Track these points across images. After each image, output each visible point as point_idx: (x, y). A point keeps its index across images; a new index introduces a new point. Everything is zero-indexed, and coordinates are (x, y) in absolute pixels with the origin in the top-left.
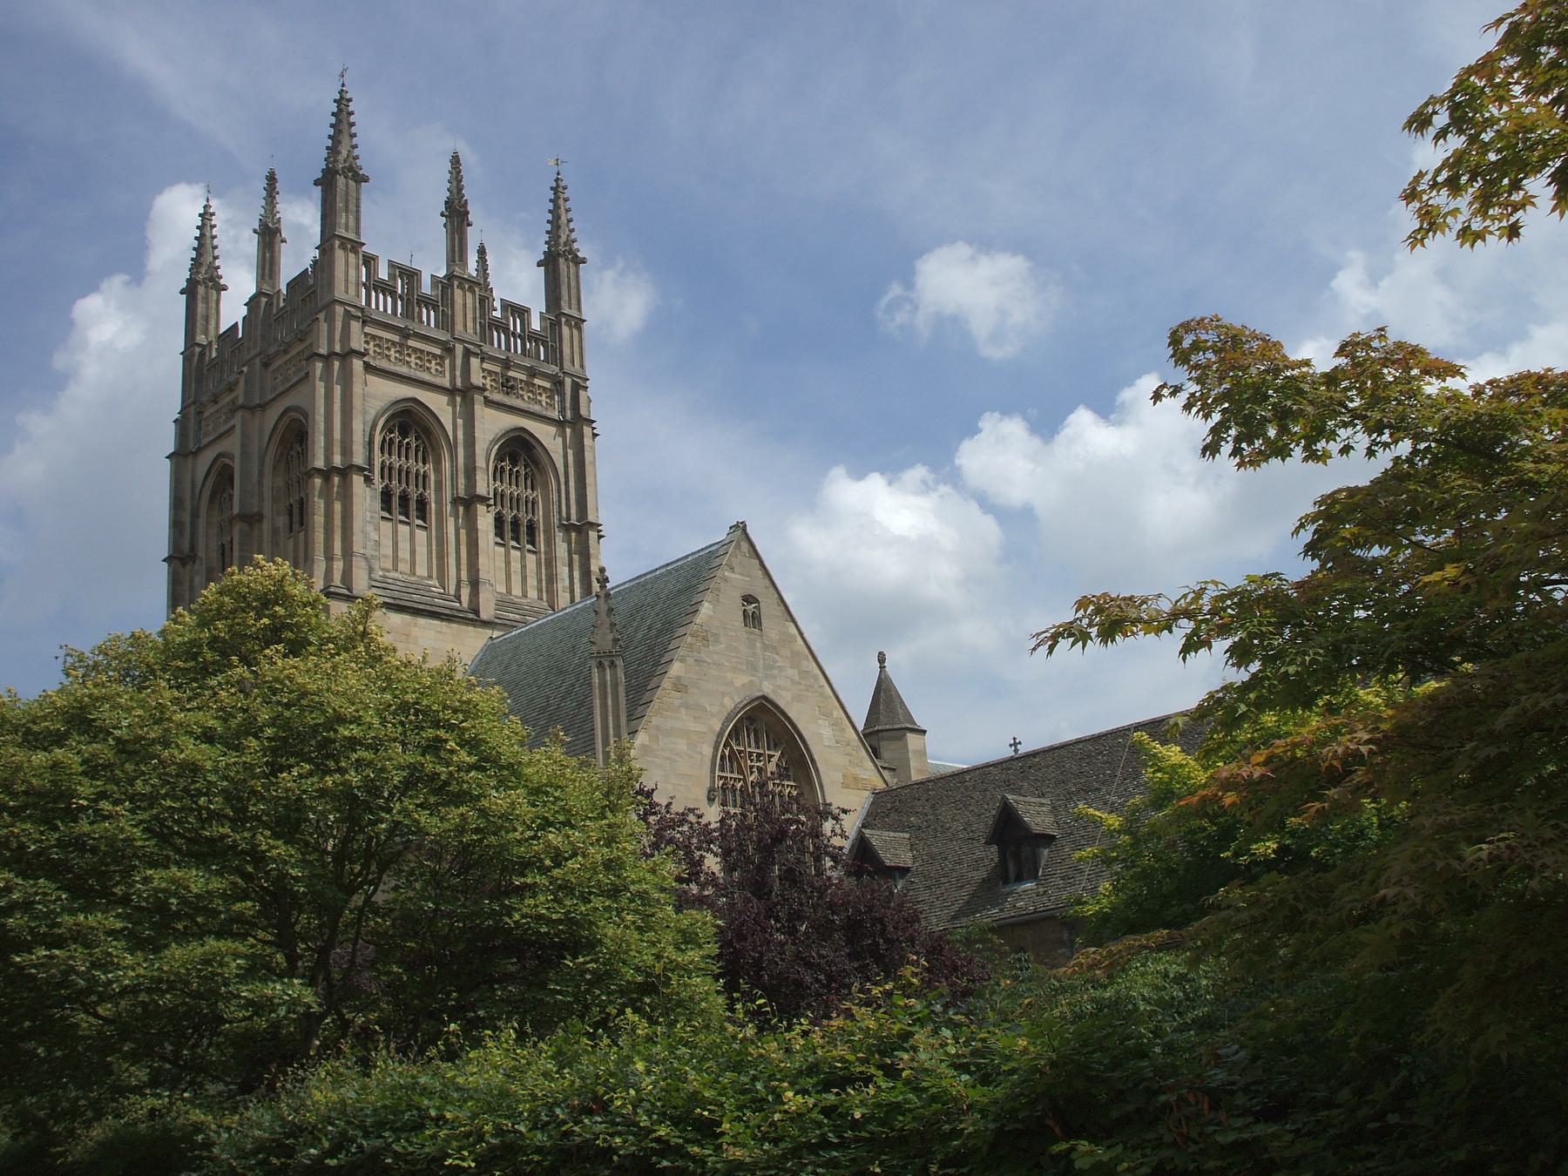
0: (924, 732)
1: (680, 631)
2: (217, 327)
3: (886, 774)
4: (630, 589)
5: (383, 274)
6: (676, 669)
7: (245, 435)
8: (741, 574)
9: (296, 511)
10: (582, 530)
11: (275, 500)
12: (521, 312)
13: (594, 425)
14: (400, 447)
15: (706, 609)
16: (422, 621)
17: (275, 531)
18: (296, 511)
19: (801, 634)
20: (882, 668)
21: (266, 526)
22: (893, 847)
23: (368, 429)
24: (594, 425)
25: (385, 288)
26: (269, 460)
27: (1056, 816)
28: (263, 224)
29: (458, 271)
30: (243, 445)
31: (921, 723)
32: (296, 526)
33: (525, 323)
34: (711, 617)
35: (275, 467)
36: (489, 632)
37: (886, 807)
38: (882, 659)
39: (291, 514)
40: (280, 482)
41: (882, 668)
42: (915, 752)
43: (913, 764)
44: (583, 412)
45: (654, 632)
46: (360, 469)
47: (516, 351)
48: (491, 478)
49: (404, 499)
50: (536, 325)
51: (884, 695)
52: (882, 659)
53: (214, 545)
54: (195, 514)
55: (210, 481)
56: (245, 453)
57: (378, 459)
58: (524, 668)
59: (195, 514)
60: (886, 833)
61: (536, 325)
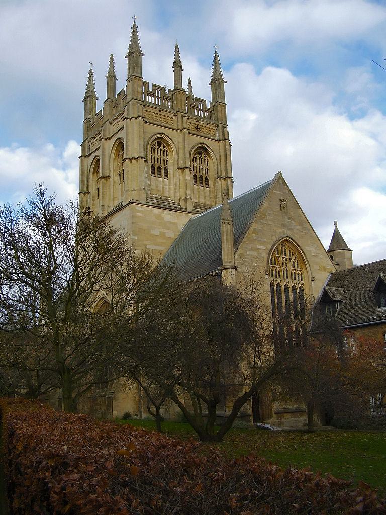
0: (352, 251)
1: (256, 212)
2: (96, 111)
3: (336, 266)
4: (239, 198)
5: (151, 89)
6: (254, 226)
7: (103, 149)
8: (280, 191)
9: (122, 174)
10: (227, 178)
11: (114, 171)
12: (203, 101)
13: (230, 142)
14: (158, 150)
15: (266, 204)
16: (166, 212)
17: (114, 182)
18: (122, 174)
19: (303, 213)
20: (336, 227)
21: (111, 180)
22: (336, 293)
23: (146, 144)
24: (230, 142)
25: (152, 94)
26: (112, 158)
27: (89, 83)
28: (109, 73)
29: (179, 86)
30: (103, 152)
31: (350, 247)
32: (122, 179)
33: (205, 105)
34: (268, 207)
35: (114, 159)
36: (190, 215)
37: (335, 279)
38: (335, 224)
39: (120, 176)
40: (116, 164)
41: (336, 227)
42: (348, 258)
43: (347, 263)
44: (226, 137)
45: (247, 213)
46: (188, 168)
47: (201, 116)
48: (192, 161)
49: (159, 168)
50: (208, 106)
51: (337, 238)
52: (335, 224)
53: (95, 188)
54: (88, 178)
55: (93, 166)
56: (103, 155)
57: (150, 155)
58: (202, 228)
59: (88, 178)
60: (334, 288)
61: (208, 106)
